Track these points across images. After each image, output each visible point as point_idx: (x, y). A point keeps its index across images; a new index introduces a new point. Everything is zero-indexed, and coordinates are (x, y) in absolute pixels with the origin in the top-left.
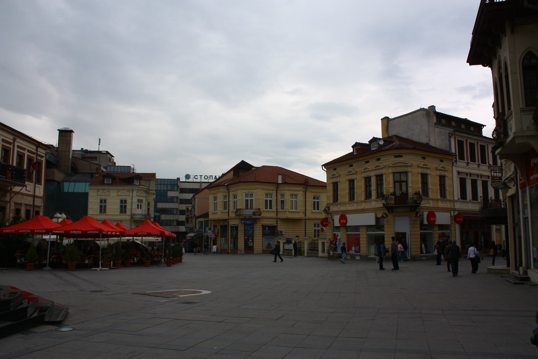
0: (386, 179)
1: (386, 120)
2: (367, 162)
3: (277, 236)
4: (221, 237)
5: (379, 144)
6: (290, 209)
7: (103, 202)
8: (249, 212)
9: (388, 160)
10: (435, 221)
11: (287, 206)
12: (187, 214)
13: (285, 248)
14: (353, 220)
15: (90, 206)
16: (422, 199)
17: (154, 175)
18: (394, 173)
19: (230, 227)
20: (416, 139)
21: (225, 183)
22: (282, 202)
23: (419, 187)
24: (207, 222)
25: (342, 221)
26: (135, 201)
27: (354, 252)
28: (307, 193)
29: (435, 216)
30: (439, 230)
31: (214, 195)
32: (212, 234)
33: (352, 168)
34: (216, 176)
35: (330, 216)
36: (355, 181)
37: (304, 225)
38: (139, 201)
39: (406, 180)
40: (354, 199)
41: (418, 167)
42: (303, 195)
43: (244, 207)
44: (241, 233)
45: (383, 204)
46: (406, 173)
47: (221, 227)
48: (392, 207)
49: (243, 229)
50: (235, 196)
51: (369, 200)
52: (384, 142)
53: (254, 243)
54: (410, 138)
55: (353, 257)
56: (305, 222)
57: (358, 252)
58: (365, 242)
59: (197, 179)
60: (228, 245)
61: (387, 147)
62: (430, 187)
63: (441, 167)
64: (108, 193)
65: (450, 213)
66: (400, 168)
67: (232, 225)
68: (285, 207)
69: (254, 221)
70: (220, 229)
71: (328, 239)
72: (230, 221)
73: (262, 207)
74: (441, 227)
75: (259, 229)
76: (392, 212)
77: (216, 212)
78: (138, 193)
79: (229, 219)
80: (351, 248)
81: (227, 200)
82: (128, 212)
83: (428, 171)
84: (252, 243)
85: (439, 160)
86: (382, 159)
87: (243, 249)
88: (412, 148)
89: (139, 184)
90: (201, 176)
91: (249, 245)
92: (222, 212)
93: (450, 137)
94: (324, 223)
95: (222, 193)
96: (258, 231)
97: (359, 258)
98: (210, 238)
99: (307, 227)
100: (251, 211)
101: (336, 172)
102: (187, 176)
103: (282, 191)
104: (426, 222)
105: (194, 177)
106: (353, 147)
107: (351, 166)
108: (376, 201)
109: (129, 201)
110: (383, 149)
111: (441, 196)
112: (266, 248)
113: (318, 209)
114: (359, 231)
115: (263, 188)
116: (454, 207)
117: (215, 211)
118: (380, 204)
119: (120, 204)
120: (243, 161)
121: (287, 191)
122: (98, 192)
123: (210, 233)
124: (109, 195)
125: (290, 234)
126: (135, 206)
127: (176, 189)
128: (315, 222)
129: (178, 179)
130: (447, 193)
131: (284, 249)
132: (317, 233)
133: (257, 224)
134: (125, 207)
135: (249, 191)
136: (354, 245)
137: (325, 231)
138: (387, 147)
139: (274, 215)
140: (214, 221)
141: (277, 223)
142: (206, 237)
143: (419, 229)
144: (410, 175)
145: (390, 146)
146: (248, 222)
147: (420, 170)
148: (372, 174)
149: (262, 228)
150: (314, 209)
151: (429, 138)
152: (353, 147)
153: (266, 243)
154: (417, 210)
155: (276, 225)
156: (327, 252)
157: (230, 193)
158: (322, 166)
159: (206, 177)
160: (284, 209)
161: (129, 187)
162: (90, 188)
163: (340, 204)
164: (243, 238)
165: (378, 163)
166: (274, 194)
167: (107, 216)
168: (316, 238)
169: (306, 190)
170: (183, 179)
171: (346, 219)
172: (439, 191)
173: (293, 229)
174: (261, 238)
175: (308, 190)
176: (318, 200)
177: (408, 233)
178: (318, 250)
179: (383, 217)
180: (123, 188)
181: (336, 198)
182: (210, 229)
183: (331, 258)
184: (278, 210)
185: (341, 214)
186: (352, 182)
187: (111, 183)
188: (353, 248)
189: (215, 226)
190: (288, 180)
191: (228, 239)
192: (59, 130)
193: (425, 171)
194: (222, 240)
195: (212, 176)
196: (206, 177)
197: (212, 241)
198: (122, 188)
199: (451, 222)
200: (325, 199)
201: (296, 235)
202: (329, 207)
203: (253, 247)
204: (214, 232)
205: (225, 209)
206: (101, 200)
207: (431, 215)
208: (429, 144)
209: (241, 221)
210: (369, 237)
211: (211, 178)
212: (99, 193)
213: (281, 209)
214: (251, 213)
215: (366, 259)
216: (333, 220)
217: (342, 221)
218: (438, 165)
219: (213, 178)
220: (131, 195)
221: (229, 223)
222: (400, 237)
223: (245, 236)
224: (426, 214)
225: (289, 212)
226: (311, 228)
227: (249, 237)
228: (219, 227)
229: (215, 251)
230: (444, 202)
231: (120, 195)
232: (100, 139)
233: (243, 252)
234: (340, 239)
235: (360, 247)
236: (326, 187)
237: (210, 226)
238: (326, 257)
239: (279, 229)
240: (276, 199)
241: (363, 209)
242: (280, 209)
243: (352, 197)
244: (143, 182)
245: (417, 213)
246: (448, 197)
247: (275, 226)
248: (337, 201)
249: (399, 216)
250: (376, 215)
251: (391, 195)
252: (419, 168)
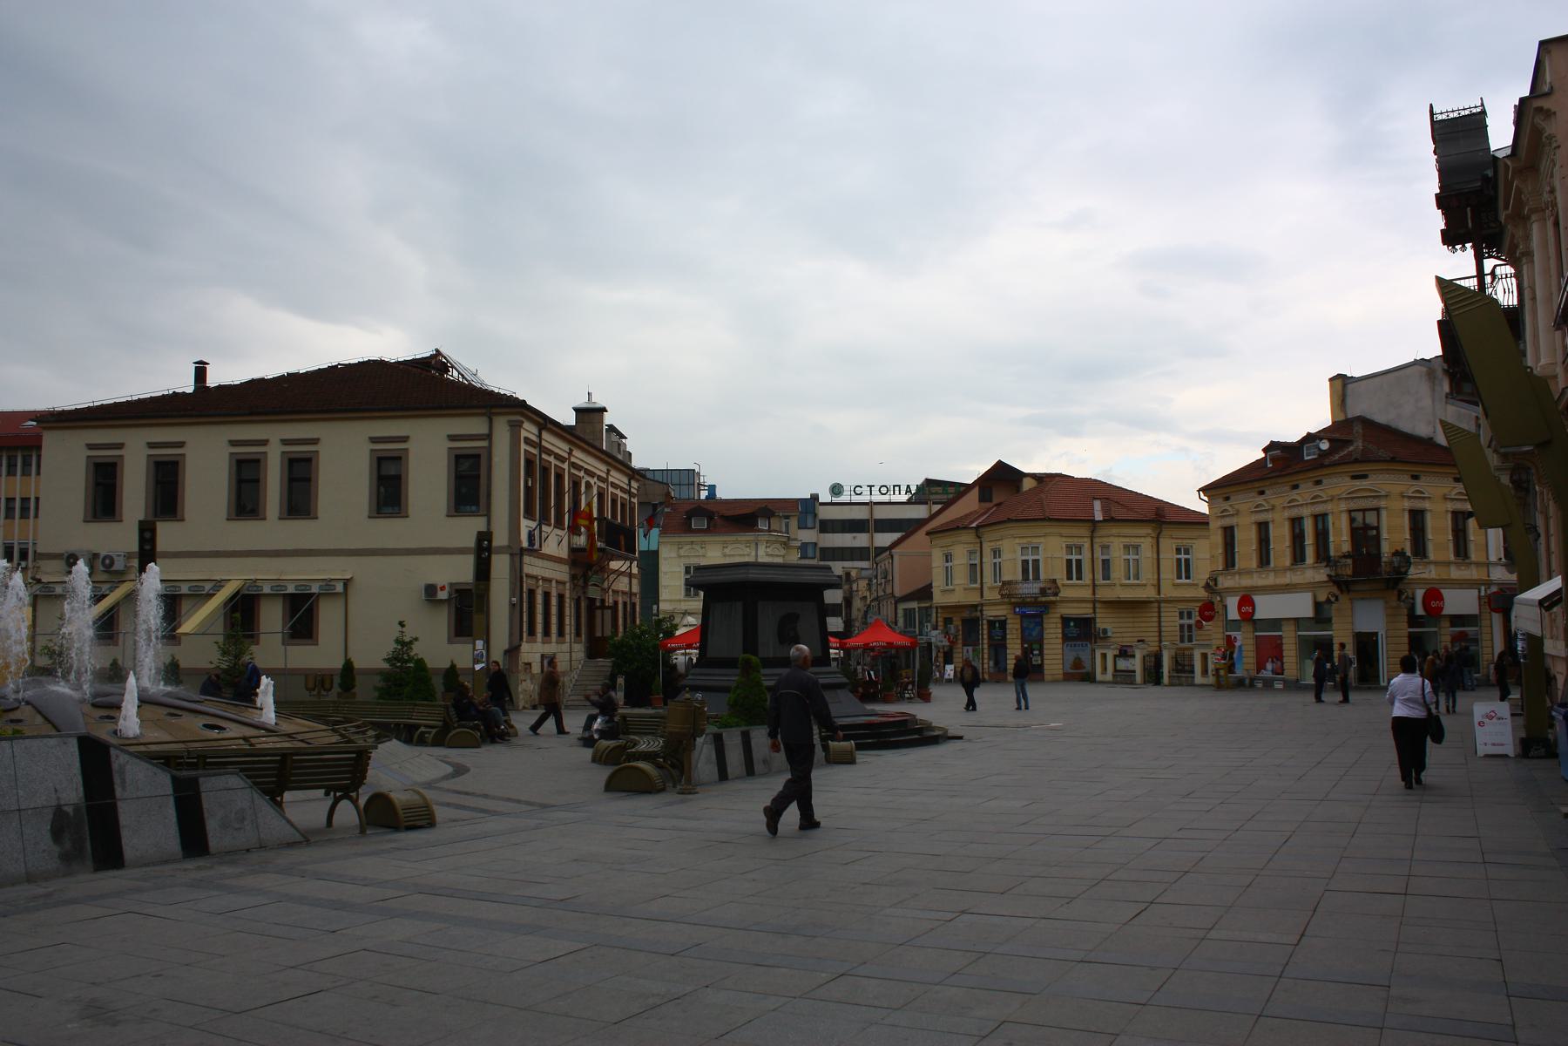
0: (1333, 524)
1: (1339, 383)
2: (1295, 487)
3: (1096, 642)
4: (964, 645)
5: (1320, 449)
6: (1123, 578)
8: (1031, 589)
9: (1339, 485)
10: (1441, 609)
11: (1117, 572)
12: (846, 587)
13: (1118, 668)
14: (1266, 607)
16: (1410, 563)
18: (1350, 511)
19: (985, 622)
20: (1405, 426)
21: (972, 522)
22: (1106, 563)
23: (1406, 539)
24: (926, 612)
25: (1244, 609)
27: (1270, 673)
28: (1161, 540)
29: (1441, 598)
30: (1452, 627)
31: (945, 549)
32: (944, 639)
33: (1263, 497)
34: (908, 486)
35: (1219, 599)
36: (1271, 526)
37: (1156, 619)
39: (1376, 525)
40: (1268, 563)
41: (1404, 497)
43: (1020, 577)
44: (1015, 636)
45: (1328, 575)
46: (1377, 510)
47: (964, 621)
48: (1347, 583)
49: (1018, 626)
50: (996, 553)
51: (1299, 566)
52: (1330, 444)
53: (1045, 657)
54: (1393, 425)
55: (1268, 684)
56: (1159, 608)
57: (1279, 674)
58: (1293, 653)
59: (860, 494)
60: (983, 664)
61: (1337, 457)
62: (1430, 537)
63: (1456, 495)
64: (701, 552)
65: (1477, 591)
67: (992, 618)
68: (1112, 575)
70: (960, 628)
71: (1214, 647)
72: (984, 608)
73: (1060, 575)
74: (1457, 620)
75: (1054, 626)
76: (1349, 591)
77: (950, 587)
78: (768, 550)
79: (982, 605)
80: (1265, 666)
81: (977, 562)
83: (1426, 505)
84: (1039, 658)
85: (1451, 479)
86: (1325, 481)
88: (1388, 458)
89: (767, 528)
90: (871, 487)
91: (1034, 663)
92: (965, 589)
94: (1207, 613)
96: (1053, 632)
97: (1281, 686)
98: (937, 647)
99: (1163, 619)
100: (1035, 585)
101: (1231, 506)
102: (836, 489)
103: (1105, 539)
104: (1420, 611)
105: (852, 489)
106: (1265, 450)
107: (1262, 493)
108: (1314, 567)
110: (1327, 462)
111: (1457, 554)
112: (1071, 669)
113: (1188, 577)
114: (1280, 630)
116: (1489, 576)
117: (947, 585)
118: (1321, 575)
120: (1000, 462)
121: (1116, 538)
122: (679, 548)
123: (936, 637)
124: (704, 556)
125: (1125, 635)
127: (810, 524)
128: (1182, 606)
129: (815, 497)
130: (1472, 547)
131: (1116, 670)
132: (1186, 633)
133: (1051, 616)
135: (1029, 539)
136: (1270, 660)
137: (1206, 628)
138: (1337, 457)
139: (1086, 593)
140: (942, 607)
141: (1094, 612)
142: (926, 645)
143: (1406, 625)
144: (1384, 514)
145: (1342, 454)
147: (1407, 504)
148: (1306, 512)
150: (1179, 577)
152: (1265, 450)
153: (1070, 658)
154: (1401, 586)
155: (1093, 615)
156: (1213, 675)
157: (985, 545)
158: (1199, 491)
159: (884, 490)
160: (1109, 579)
161: (749, 536)
163: (1240, 574)
164: (1019, 646)
165: (1316, 490)
166: (1087, 546)
168: (1186, 644)
169: (1159, 534)
170: (825, 497)
171: (1252, 604)
172: (1451, 546)
173: (1131, 625)
174: (1060, 646)
175: (1164, 533)
176: (1186, 556)
177: (1382, 632)
178: (1193, 672)
179: (1328, 601)
181: (1229, 561)
182: (936, 628)
183: (1220, 686)
185: (1241, 594)
186: (1263, 528)
188: (1269, 666)
189: (948, 621)
190: (1118, 513)
191: (983, 649)
192: (575, 409)
193: (1419, 505)
194: (968, 651)
195: (899, 486)
196: (884, 490)
197: (941, 655)
198: (733, 538)
199: (1480, 609)
200: (1205, 554)
201: (1140, 638)
203: (1041, 667)
204: (946, 633)
205: (973, 580)
206: (686, 567)
207: (1433, 595)
208: (1435, 439)
209: (1015, 610)
210: (1302, 641)
211: (897, 492)
212: (682, 552)
214: (1037, 591)
215: (1295, 686)
216: (1226, 607)
217: (1244, 609)
218: (1449, 489)
219: (903, 492)
221: (984, 613)
222: (1366, 645)
223: (1023, 641)
224: (1420, 594)
225: (1122, 585)
226: (1172, 621)
227: (1034, 643)
228: (960, 623)
229: (952, 677)
230: (1463, 568)
231: (729, 556)
234: (1240, 647)
235: (1282, 664)
236: (1208, 524)
237: (934, 619)
238: (1211, 685)
239: (1100, 624)
241: (1287, 585)
242: (1100, 581)
243: (1264, 559)
244: (775, 523)
245: (1400, 593)
246: (1474, 556)
248: (1233, 565)
249: (1362, 599)
250: (1315, 597)
251: (1345, 556)
252: (1406, 499)
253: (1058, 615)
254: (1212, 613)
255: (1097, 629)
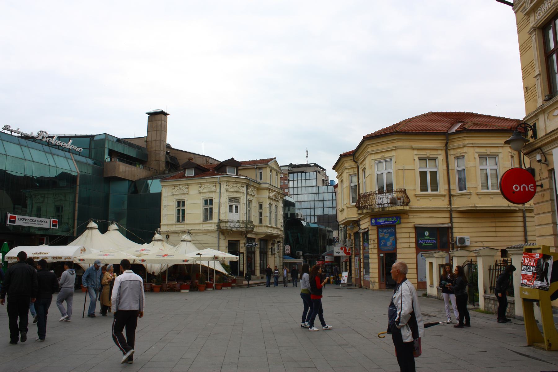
7: (181, 204)
8: (384, 199)
15: (164, 212)
17: (273, 160)
26: (225, 199)
32: (340, 251)
37: (521, 224)
38: (231, 199)
42: (512, 157)
56: (524, 217)
68: (468, 185)
69: (395, 219)
75: (407, 235)
82: (215, 219)
87: (377, 280)
89: (235, 174)
94: (517, 188)
103: (459, 150)
109: (215, 201)
115: (412, 146)
119: (204, 206)
126: (225, 208)
133: (403, 225)
134: (211, 209)
139: (443, 203)
141: (451, 222)
146: (384, 221)
149: (416, 233)
155: (450, 225)
162: (162, 185)
167: (186, 226)
173: (494, 234)
174: (414, 255)
180: (205, 181)
184: (452, 193)
187: (194, 175)
192: (148, 114)
202: (534, 125)
213: (460, 189)
220: (218, 190)
225: (478, 194)
232: (307, 151)
233: (377, 286)
239: (457, 234)
240: (445, 168)
247: (448, 228)
253: (411, 225)
254: (530, 187)
255: (455, 239)
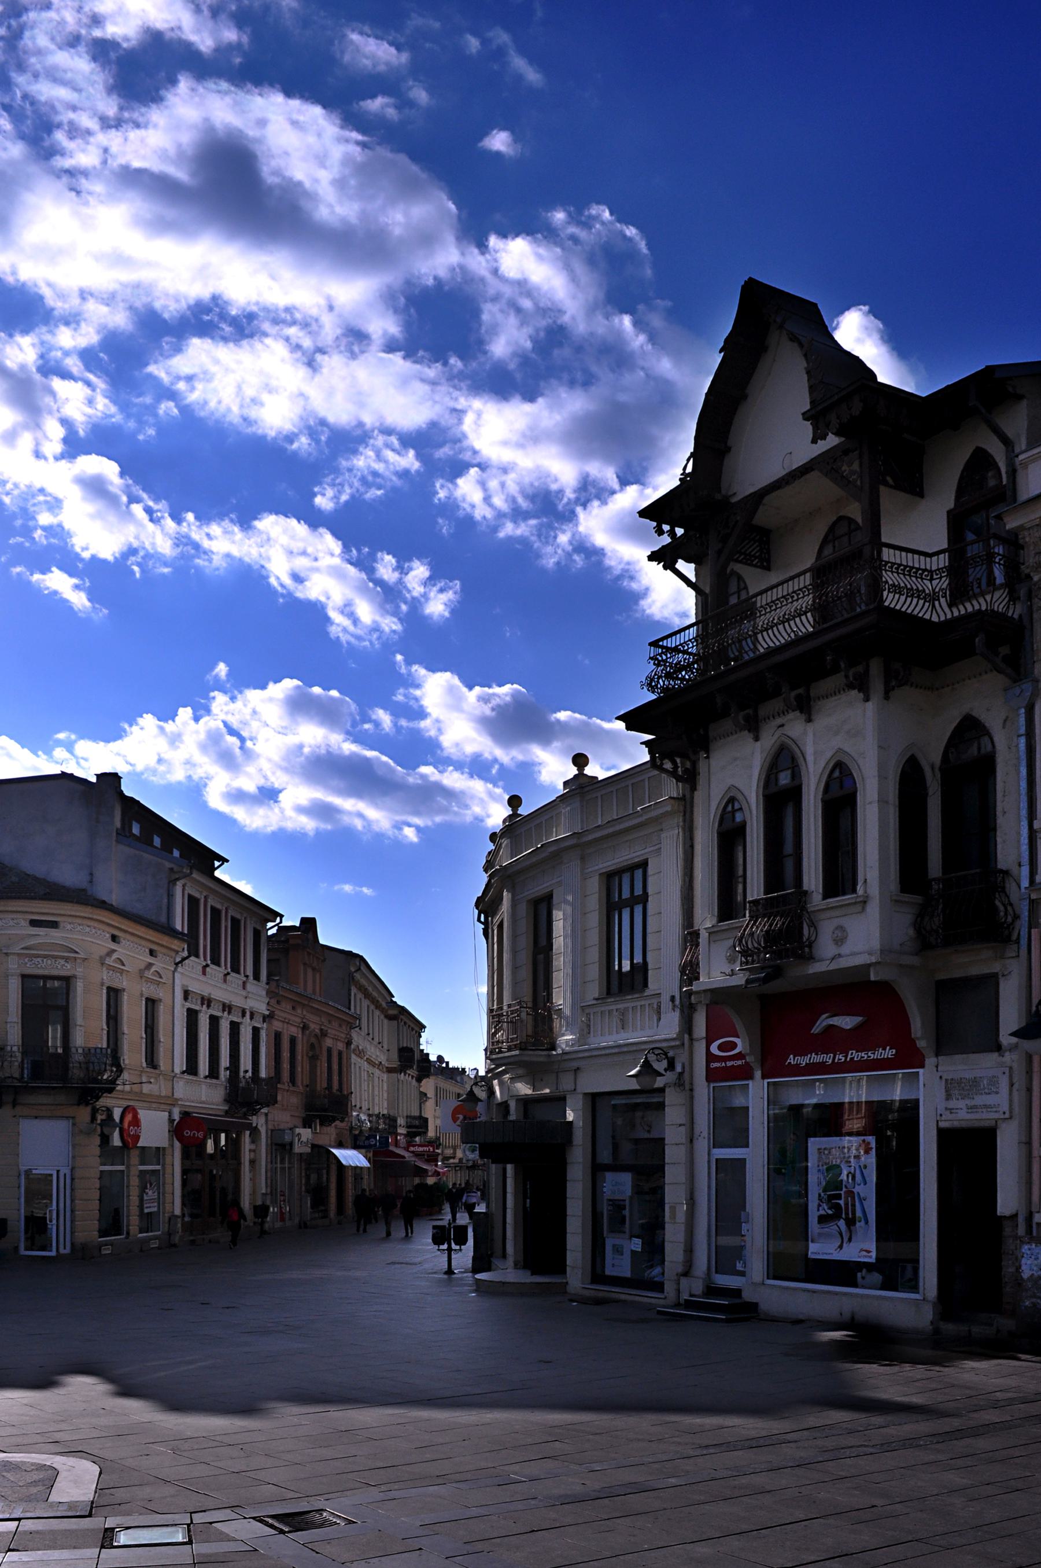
10: (137, 1138)
17: (756, 1305)
30: (141, 1164)
62: (79, 1021)
66: (49, 962)
93: (173, 882)
95: (65, 1170)
151: (91, 874)
